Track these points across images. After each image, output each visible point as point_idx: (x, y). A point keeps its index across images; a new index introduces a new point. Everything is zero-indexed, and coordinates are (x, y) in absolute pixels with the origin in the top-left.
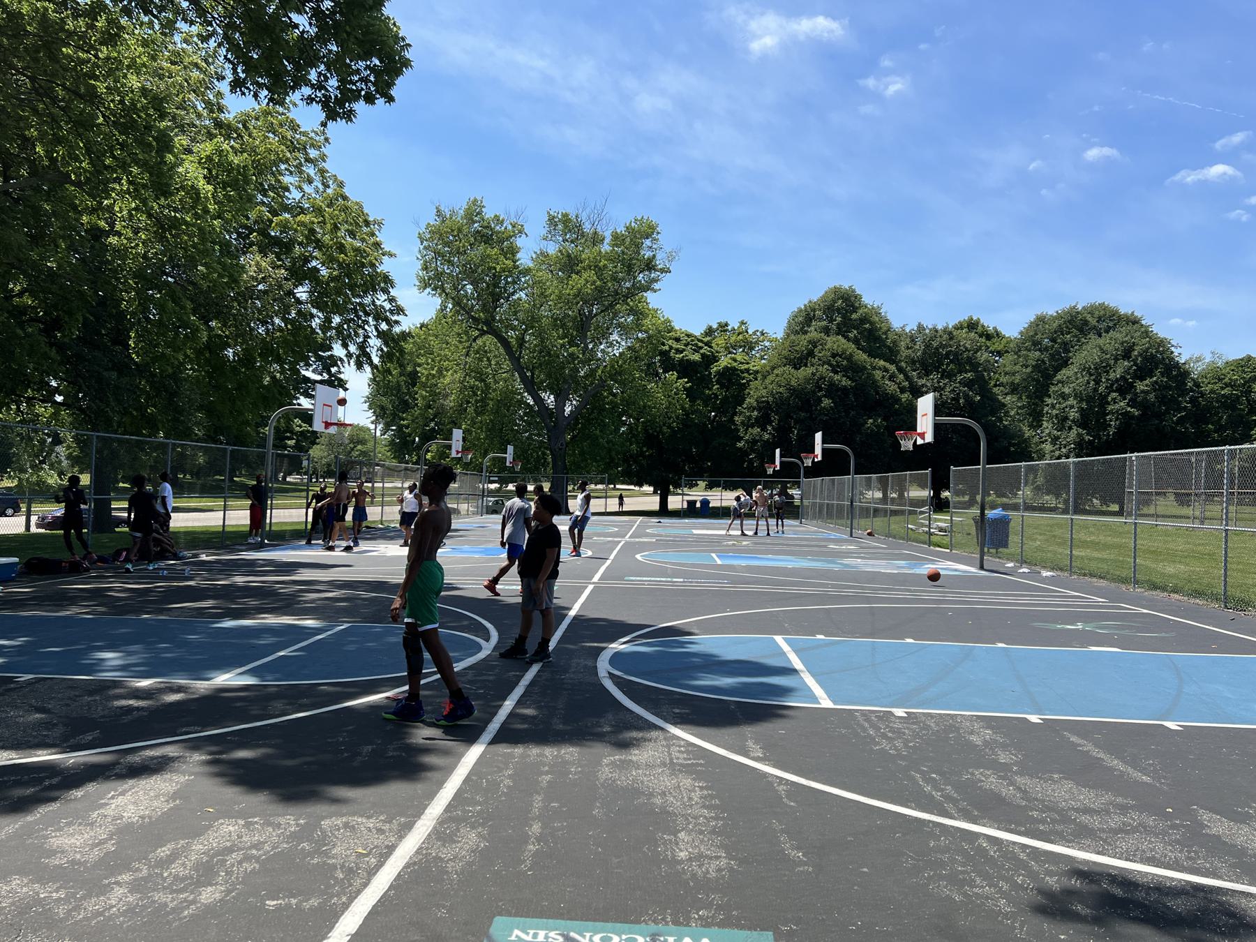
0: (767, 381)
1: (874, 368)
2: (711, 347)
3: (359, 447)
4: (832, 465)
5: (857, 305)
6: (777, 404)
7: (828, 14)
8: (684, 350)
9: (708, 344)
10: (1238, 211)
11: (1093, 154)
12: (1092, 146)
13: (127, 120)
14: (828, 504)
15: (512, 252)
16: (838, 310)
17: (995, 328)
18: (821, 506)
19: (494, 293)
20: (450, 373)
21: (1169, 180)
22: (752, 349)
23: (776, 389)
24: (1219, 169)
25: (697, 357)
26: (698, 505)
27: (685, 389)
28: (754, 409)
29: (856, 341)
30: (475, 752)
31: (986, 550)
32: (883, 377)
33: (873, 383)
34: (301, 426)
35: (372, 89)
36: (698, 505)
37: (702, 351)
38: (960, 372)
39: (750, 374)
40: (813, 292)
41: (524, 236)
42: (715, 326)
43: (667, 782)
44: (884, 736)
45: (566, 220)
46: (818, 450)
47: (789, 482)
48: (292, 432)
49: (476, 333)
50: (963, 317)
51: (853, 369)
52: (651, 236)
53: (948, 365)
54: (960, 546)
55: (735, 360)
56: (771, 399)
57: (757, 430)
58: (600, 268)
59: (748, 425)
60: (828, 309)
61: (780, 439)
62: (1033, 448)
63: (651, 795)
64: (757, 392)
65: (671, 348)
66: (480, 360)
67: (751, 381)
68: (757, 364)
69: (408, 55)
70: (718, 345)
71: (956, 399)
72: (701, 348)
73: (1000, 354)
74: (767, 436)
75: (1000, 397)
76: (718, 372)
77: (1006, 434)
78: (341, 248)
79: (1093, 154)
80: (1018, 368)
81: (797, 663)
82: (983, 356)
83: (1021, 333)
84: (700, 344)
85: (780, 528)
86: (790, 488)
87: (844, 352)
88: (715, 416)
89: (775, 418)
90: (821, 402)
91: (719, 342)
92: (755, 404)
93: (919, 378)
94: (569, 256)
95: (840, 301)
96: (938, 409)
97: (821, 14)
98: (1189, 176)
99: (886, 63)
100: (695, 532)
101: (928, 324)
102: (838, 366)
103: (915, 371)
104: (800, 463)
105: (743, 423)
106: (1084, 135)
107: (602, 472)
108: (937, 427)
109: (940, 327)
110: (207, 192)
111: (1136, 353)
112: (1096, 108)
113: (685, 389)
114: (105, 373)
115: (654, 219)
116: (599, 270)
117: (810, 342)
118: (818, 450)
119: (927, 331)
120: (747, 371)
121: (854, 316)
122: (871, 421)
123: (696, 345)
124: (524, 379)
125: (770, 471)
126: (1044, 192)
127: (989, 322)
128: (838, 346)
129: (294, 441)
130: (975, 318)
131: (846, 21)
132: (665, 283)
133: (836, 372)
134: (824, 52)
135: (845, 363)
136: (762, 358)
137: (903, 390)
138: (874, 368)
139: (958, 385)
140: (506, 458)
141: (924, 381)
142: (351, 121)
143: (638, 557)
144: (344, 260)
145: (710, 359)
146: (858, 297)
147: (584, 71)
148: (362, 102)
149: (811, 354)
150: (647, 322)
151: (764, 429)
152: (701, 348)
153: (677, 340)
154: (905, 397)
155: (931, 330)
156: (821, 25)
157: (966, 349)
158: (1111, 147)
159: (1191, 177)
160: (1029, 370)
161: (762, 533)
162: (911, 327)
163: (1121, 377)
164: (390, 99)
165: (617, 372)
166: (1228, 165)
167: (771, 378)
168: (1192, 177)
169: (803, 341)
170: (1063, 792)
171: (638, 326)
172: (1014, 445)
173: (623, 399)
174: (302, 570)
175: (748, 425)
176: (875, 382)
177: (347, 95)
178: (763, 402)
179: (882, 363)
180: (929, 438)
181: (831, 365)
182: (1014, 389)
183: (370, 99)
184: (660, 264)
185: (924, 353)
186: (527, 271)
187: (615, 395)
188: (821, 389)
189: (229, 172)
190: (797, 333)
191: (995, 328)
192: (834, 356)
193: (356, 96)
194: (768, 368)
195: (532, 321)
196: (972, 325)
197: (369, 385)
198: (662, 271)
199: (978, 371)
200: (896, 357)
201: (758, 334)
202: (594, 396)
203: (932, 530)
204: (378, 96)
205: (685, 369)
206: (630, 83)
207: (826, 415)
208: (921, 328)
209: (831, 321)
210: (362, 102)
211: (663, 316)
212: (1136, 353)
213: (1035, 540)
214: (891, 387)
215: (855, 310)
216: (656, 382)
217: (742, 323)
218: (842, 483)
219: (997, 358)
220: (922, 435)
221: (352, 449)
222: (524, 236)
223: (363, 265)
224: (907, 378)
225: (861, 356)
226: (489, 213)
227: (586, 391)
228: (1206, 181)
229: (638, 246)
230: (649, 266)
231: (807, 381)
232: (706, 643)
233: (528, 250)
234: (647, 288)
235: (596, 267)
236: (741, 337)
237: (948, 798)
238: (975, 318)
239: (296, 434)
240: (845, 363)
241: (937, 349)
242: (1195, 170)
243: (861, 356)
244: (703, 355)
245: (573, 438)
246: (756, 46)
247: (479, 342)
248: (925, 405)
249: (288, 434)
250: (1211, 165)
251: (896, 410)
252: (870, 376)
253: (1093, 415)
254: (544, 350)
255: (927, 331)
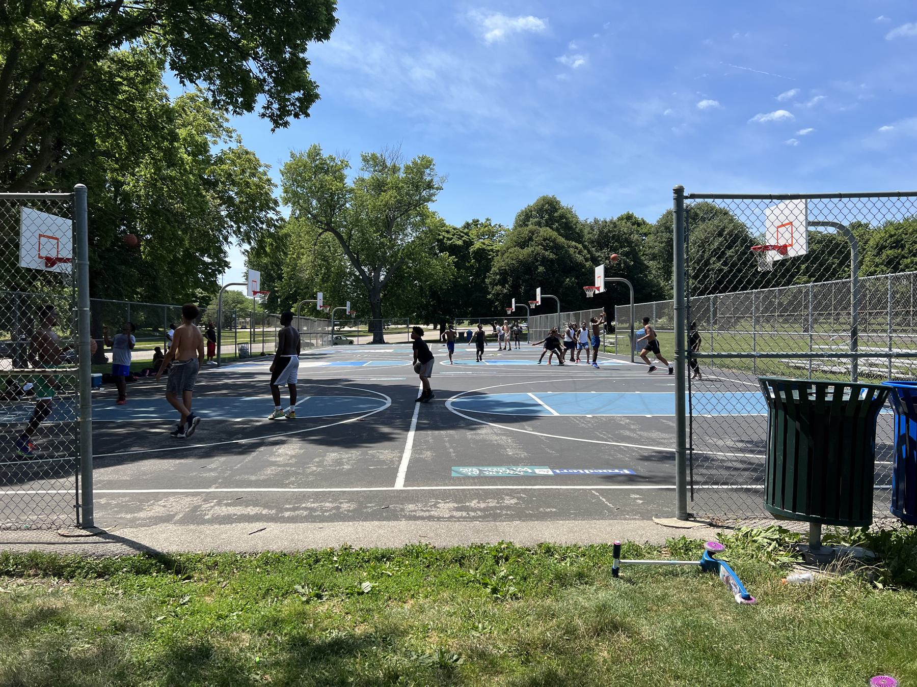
0: (505, 257)
1: (569, 247)
2: (468, 236)
3: (239, 306)
4: (547, 307)
5: (557, 207)
6: (511, 271)
7: (535, 16)
8: (452, 238)
9: (467, 234)
10: (793, 139)
11: (703, 104)
12: (702, 99)
13: (153, 125)
14: (544, 331)
15: (341, 179)
16: (546, 210)
17: (642, 219)
18: (540, 332)
19: (331, 203)
20: (305, 256)
21: (750, 120)
22: (493, 236)
23: (510, 262)
24: (780, 113)
25: (460, 243)
26: (465, 335)
27: (454, 262)
28: (497, 274)
29: (557, 230)
30: (411, 435)
31: (636, 352)
32: (575, 252)
33: (569, 256)
34: (202, 293)
35: (298, 109)
36: (465, 335)
37: (463, 239)
38: (621, 247)
39: (493, 253)
40: (530, 201)
41: (349, 168)
42: (470, 222)
43: (495, 438)
44: (583, 423)
45: (374, 158)
46: (538, 298)
47: (519, 319)
48: (196, 297)
49: (321, 231)
50: (623, 212)
51: (557, 248)
52: (429, 167)
53: (613, 243)
54: (622, 351)
55: (484, 244)
56: (507, 268)
57: (499, 287)
58: (399, 189)
59: (494, 284)
60: (540, 210)
61: (514, 293)
62: (666, 293)
63: (492, 441)
64: (498, 264)
65: (444, 237)
66: (324, 247)
67: (494, 256)
68: (498, 246)
69: (318, 91)
70: (472, 234)
71: (619, 264)
72: (463, 237)
73: (646, 235)
74: (506, 291)
75: (645, 262)
76: (474, 252)
77: (650, 284)
78: (247, 184)
79: (703, 104)
80: (657, 244)
81: (540, 402)
82: (635, 237)
83: (658, 222)
84: (462, 234)
85: (518, 346)
86: (521, 323)
87: (550, 237)
88: (472, 279)
89: (510, 279)
90: (538, 269)
91: (473, 232)
92: (498, 271)
93: (597, 251)
94: (378, 180)
95: (547, 205)
96: (607, 274)
97: (532, 15)
98: (762, 117)
99: (573, 46)
100: (468, 350)
101: (601, 219)
102: (547, 246)
103: (594, 247)
104: (527, 307)
105: (490, 283)
106: (698, 93)
107: (405, 316)
108: (607, 284)
109: (608, 220)
110: (188, 160)
111: (726, 232)
112: (705, 75)
113: (454, 262)
114: (117, 267)
115: (430, 156)
116: (398, 189)
117: (530, 231)
118: (538, 298)
119: (600, 222)
120: (492, 250)
121: (556, 214)
122: (568, 279)
123: (459, 235)
124: (352, 258)
125: (509, 312)
126: (674, 129)
127: (639, 215)
128: (547, 234)
129: (198, 303)
130: (630, 213)
131: (547, 20)
132: (439, 197)
133: (547, 250)
134: (532, 40)
135: (551, 244)
136: (500, 241)
137: (587, 260)
138: (569, 247)
139: (620, 255)
140: (346, 310)
141: (599, 254)
142: (287, 127)
143: (441, 363)
144: (250, 192)
145: (469, 244)
146: (558, 203)
147: (377, 53)
148: (292, 117)
149: (531, 239)
150: (428, 221)
151: (504, 287)
152: (463, 237)
153: (448, 232)
154: (588, 264)
155: (602, 222)
156: (531, 23)
157: (624, 233)
158: (714, 100)
159: (763, 118)
160: (664, 245)
161: (508, 347)
162: (591, 220)
163: (717, 248)
164: (307, 115)
165: (411, 252)
166: (786, 110)
167: (506, 255)
168: (764, 118)
169: (525, 231)
170: (655, 435)
171: (423, 222)
172: (654, 291)
173: (415, 270)
174: (256, 376)
175: (494, 284)
176: (570, 255)
177: (284, 112)
178: (503, 269)
179: (574, 243)
180: (602, 290)
181: (543, 246)
182: (654, 257)
183: (296, 116)
184: (436, 184)
185: (599, 235)
186: (351, 191)
187: (410, 268)
188: (537, 261)
189: (196, 146)
190: (521, 226)
191: (642, 219)
192: (545, 240)
193: (289, 113)
194: (505, 248)
195: (357, 222)
196: (629, 217)
197: (245, 265)
198: (438, 189)
199: (632, 247)
200: (582, 239)
201: (497, 226)
202: (398, 268)
203: (606, 344)
204: (301, 113)
205: (453, 250)
206: (408, 61)
207: (541, 277)
208: (596, 221)
209: (542, 218)
210: (292, 117)
211: (439, 217)
212: (726, 232)
213: (665, 347)
214: (580, 258)
215: (556, 210)
216: (436, 259)
217: (488, 220)
218: (552, 318)
219: (644, 238)
220: (598, 289)
221: (234, 307)
222: (349, 168)
223: (262, 194)
224: (589, 252)
225: (561, 240)
226: (325, 154)
227: (392, 265)
228: (772, 120)
229: (422, 173)
230: (429, 186)
231: (529, 255)
232: (493, 397)
233: (351, 178)
234: (428, 200)
235: (396, 187)
236: (487, 228)
237: (609, 438)
238: (630, 213)
239: (199, 298)
240: (551, 244)
241: (606, 233)
242: (766, 114)
243: (561, 240)
244: (464, 241)
245: (385, 295)
246: (489, 36)
247: (322, 236)
248: (599, 271)
249: (194, 299)
250: (775, 111)
251: (583, 272)
252: (567, 251)
253: (701, 272)
254: (365, 240)
255: (600, 222)
